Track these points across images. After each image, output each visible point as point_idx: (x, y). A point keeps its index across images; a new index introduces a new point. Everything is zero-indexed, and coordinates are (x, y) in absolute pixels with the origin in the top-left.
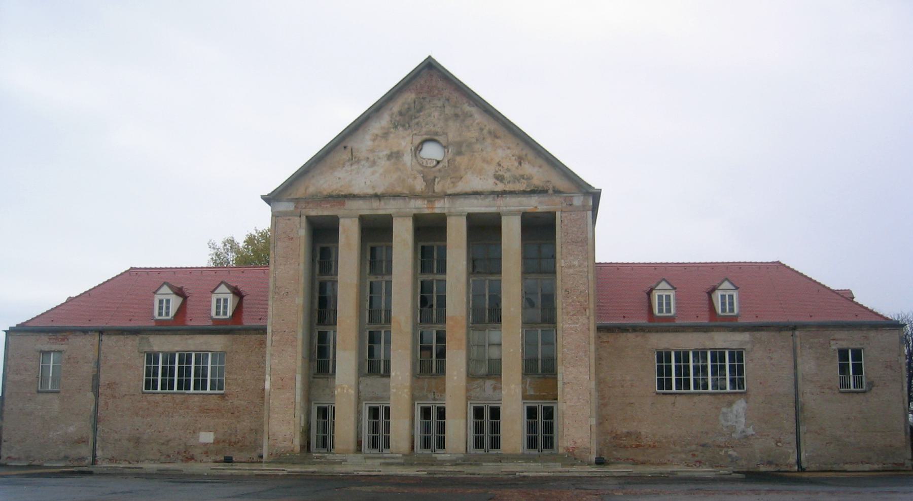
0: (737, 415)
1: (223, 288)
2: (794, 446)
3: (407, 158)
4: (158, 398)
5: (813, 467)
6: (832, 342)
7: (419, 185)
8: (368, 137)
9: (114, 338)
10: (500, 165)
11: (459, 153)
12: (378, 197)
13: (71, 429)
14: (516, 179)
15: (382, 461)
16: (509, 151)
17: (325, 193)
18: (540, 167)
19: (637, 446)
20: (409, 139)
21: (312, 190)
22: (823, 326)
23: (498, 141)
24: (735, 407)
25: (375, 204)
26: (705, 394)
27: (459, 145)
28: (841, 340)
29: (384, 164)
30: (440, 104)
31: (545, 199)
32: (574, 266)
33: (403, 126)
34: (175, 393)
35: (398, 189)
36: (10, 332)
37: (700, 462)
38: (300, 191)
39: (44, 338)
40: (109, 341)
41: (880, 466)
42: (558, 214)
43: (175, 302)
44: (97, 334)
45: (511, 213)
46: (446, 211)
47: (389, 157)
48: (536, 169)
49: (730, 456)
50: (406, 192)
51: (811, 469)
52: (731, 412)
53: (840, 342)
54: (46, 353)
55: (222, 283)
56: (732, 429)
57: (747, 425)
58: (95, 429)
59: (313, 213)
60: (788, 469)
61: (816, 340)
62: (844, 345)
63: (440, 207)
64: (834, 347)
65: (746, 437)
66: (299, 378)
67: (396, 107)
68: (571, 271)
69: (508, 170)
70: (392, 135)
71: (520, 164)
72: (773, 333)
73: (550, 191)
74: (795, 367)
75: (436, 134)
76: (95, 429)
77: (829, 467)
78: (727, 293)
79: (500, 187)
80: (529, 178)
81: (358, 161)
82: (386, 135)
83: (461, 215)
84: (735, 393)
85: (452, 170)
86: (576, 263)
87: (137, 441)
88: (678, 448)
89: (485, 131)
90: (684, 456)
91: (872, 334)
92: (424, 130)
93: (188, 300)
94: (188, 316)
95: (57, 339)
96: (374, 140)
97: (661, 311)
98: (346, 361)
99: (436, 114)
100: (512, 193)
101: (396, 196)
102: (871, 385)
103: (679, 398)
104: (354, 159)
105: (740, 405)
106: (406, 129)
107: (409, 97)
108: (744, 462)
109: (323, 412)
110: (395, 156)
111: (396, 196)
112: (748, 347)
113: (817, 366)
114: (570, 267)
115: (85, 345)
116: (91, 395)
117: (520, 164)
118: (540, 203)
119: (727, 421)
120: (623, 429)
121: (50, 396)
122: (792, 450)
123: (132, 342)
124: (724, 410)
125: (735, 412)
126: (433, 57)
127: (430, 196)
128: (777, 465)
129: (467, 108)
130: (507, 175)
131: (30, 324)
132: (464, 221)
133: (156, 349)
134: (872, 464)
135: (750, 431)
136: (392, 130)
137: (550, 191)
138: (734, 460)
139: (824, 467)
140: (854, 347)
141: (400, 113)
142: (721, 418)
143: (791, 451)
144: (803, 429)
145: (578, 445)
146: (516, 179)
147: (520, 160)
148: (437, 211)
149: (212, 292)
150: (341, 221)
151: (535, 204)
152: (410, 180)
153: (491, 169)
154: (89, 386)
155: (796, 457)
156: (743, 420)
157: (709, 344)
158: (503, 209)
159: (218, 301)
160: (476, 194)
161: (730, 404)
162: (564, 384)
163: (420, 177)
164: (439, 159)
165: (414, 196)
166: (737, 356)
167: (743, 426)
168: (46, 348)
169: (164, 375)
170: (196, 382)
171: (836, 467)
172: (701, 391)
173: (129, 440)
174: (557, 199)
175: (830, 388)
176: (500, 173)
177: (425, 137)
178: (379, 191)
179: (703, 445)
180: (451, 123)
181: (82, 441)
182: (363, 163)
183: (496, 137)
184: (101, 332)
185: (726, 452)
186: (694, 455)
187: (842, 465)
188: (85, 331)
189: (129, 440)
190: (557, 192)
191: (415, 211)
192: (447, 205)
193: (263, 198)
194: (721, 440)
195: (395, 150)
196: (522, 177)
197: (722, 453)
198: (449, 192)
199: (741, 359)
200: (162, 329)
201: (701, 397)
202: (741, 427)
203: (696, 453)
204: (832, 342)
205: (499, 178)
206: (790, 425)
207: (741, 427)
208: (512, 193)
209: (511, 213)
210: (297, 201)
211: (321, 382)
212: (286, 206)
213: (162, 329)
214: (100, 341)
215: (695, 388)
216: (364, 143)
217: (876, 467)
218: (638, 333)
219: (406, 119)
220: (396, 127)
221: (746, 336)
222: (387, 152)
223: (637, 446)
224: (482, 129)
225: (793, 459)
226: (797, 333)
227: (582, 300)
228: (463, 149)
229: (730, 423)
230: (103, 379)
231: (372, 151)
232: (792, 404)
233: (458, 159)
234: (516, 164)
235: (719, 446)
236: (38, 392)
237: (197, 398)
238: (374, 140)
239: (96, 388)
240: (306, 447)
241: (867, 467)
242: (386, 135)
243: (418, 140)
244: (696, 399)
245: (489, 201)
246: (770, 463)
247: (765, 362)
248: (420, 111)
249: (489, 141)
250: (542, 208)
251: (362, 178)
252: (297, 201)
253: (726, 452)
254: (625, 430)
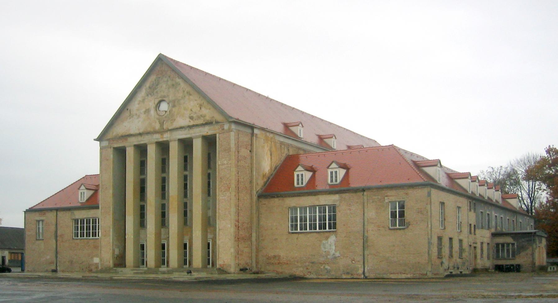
0: (331, 244)
1: (334, 165)
2: (362, 263)
3: (152, 112)
4: (78, 241)
5: (372, 276)
6: (386, 198)
7: (157, 126)
8: (136, 102)
9: (62, 213)
10: (191, 110)
11: (174, 106)
12: (140, 134)
13: (48, 257)
14: (199, 117)
15: (136, 271)
16: (196, 102)
17: (120, 135)
18: (210, 109)
19: (279, 263)
20: (153, 102)
21: (115, 134)
22: (380, 188)
23: (191, 97)
24: (330, 240)
25: (140, 138)
26: (296, 233)
27: (174, 101)
28: (391, 196)
29: (143, 116)
30: (165, 79)
31: (212, 127)
32: (224, 164)
33: (151, 94)
34: (327, 232)
35: (149, 129)
36: (26, 212)
37: (310, 272)
38: (111, 135)
39: (37, 214)
40: (60, 214)
41: (412, 275)
42: (217, 136)
43: (342, 173)
44: (55, 212)
45: (197, 137)
46: (168, 139)
47: (145, 112)
48: (208, 111)
49: (326, 269)
50: (152, 130)
51: (371, 277)
52: (328, 243)
53: (390, 198)
54: (39, 221)
55: (333, 162)
56: (328, 253)
57: (336, 251)
58: (57, 257)
59: (115, 146)
60: (358, 277)
61: (376, 197)
62: (393, 199)
63: (166, 137)
64: (386, 201)
65: (335, 258)
66: (111, 230)
67: (147, 84)
68: (223, 167)
69: (195, 113)
70: (146, 100)
71: (201, 108)
72: (352, 194)
73: (214, 123)
74: (364, 214)
75: (164, 97)
76: (57, 257)
77: (381, 276)
78: (334, 171)
79: (192, 123)
80: (204, 116)
81: (132, 117)
82: (144, 100)
83: (175, 141)
84: (321, 232)
85: (170, 116)
86: (225, 162)
87: (71, 262)
88: (299, 264)
89: (185, 92)
90: (302, 269)
91: (410, 191)
92: (159, 95)
93: (350, 171)
94: (317, 183)
95: (272, 175)
96: (139, 104)
97: (298, 184)
98: (174, 219)
99: (164, 86)
100: (197, 126)
101: (148, 133)
102: (409, 224)
103: (300, 235)
104: (131, 116)
105: (332, 239)
106: (152, 96)
107: (153, 78)
108: (333, 273)
109: (142, 247)
110: (147, 111)
111: (148, 133)
112: (337, 203)
113: (376, 214)
114: (223, 164)
115: (51, 216)
116: (54, 241)
117: (201, 108)
118: (209, 130)
119: (325, 248)
120: (271, 254)
121: (41, 241)
122: (360, 266)
123: (68, 214)
124: (324, 242)
125: (329, 243)
126: (162, 53)
127: (162, 132)
128: (352, 275)
129: (178, 80)
130: (194, 116)
131: (35, 208)
132: (176, 143)
133: (77, 217)
134: (407, 274)
135: (338, 254)
136: (146, 97)
137: (214, 123)
138: (328, 272)
139: (378, 276)
140: (399, 200)
141: (150, 88)
142: (322, 247)
143: (360, 266)
144: (366, 253)
145: (226, 263)
146: (199, 117)
147: (201, 106)
148: (165, 139)
149: (328, 168)
150: (127, 149)
151: (207, 131)
152: (153, 124)
153: (187, 113)
154: (53, 237)
155: (362, 269)
156: (334, 248)
157: (317, 203)
158: (193, 135)
159: (332, 173)
160: (181, 128)
161: (327, 238)
162: (219, 230)
163: (157, 121)
164: (166, 110)
165: (156, 132)
166: (333, 208)
167: (333, 252)
168: (38, 218)
169: (330, 220)
170: (310, 225)
171: (385, 276)
172: (313, 231)
173: (69, 262)
174: (217, 127)
175: (383, 227)
176: (192, 115)
177: (160, 99)
178: (141, 131)
179: (313, 263)
180: (170, 90)
181: (52, 263)
182: (134, 117)
183: (190, 95)
184: (57, 210)
185: (324, 267)
186: (307, 268)
187: (388, 275)
188: (51, 210)
189: (69, 262)
190: (217, 122)
191: (156, 140)
192: (169, 136)
193: (95, 140)
194: (322, 259)
195: (147, 108)
196: (201, 116)
197: (322, 267)
198: (170, 128)
199: (334, 212)
200: (82, 207)
201: (312, 234)
202: (332, 252)
203: (309, 267)
204: (386, 198)
205: (191, 118)
206: (359, 250)
207: (332, 252)
208: (197, 126)
209: (197, 137)
210: (108, 140)
211: (142, 232)
212: (105, 143)
213: (82, 207)
214: (57, 214)
215: (329, 229)
216: (134, 106)
217: (409, 276)
218: (280, 198)
219: (152, 90)
220: (148, 95)
221: (336, 197)
222: (144, 110)
223: (279, 263)
224: (184, 91)
225: (361, 271)
226: (365, 193)
227: (228, 183)
228: (176, 103)
229: (326, 250)
230: (59, 233)
231: (138, 110)
232: (362, 237)
233: (174, 109)
234: (199, 109)
235: (320, 263)
236: (37, 240)
237: (92, 241)
238: (139, 104)
239: (56, 237)
240: (117, 265)
241: (404, 276)
242: (144, 100)
243: (156, 102)
244: (309, 235)
245: (186, 131)
246: (348, 273)
247: (349, 211)
248: (157, 85)
249: (187, 97)
250: (210, 133)
251: (132, 126)
252: (108, 140)
253: (324, 267)
254: (273, 254)
